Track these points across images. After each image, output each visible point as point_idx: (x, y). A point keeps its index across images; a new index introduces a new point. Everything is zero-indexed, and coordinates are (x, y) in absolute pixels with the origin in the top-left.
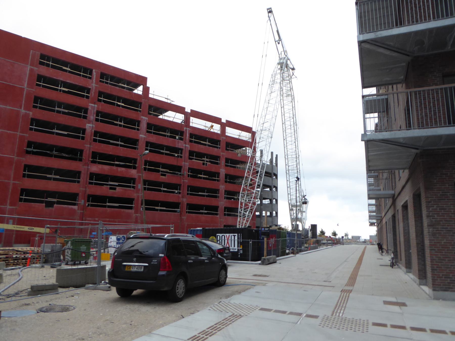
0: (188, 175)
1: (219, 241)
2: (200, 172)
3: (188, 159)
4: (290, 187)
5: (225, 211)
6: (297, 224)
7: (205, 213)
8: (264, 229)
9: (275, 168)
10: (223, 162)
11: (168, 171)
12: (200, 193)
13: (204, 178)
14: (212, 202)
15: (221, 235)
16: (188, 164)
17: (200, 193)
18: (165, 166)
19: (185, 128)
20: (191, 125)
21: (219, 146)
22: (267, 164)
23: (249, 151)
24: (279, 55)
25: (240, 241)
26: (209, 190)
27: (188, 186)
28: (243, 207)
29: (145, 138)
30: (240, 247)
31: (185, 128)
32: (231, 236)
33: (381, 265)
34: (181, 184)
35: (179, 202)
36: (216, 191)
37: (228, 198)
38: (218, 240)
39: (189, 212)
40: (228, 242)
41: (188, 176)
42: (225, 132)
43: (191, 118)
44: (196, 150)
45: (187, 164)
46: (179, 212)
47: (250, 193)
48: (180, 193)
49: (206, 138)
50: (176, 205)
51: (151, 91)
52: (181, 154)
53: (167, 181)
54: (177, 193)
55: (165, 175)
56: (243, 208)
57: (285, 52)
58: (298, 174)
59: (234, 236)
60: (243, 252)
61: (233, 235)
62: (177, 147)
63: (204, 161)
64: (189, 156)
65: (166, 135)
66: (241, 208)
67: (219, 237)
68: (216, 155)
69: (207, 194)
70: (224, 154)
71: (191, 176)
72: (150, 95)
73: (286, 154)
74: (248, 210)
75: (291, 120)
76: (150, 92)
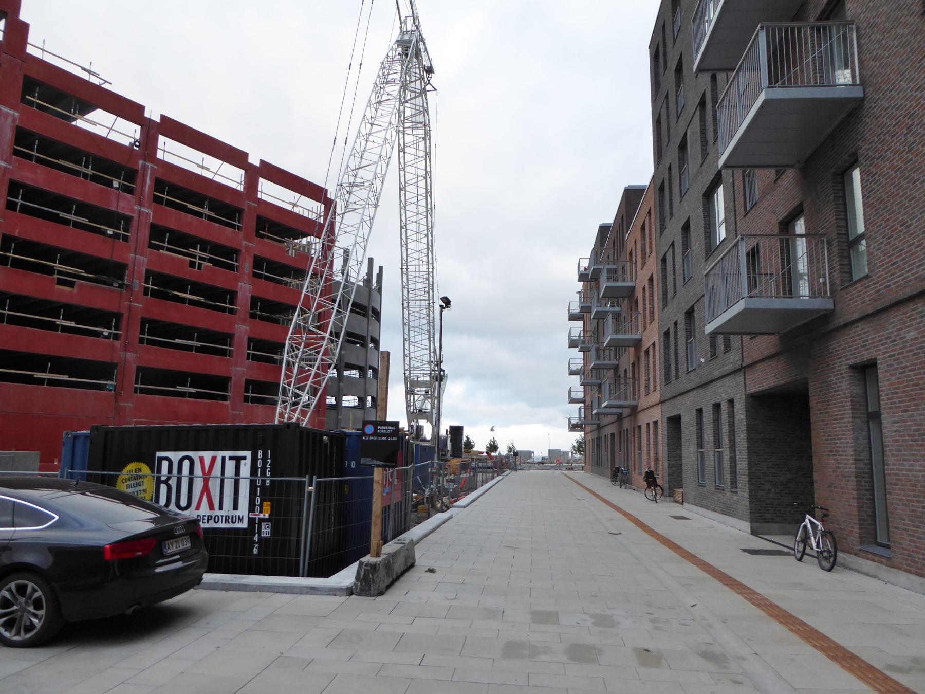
0: (146, 289)
1: (166, 482)
2: (181, 285)
3: (146, 246)
4: (409, 339)
5: (247, 391)
6: (420, 424)
7: (190, 393)
8: (376, 429)
9: (375, 294)
10: (247, 266)
11: (82, 272)
12: (177, 341)
13: (192, 302)
14: (214, 366)
15: (175, 456)
16: (146, 259)
17: (177, 341)
18: (70, 258)
19: (141, 162)
20: (160, 155)
21: (237, 223)
22: (358, 285)
23: (314, 244)
24: (401, 23)
25: (263, 482)
26: (205, 335)
27: (144, 322)
28: (295, 375)
29: (5, 168)
30: (261, 512)
31: (141, 162)
32: (224, 458)
33: (745, 551)
34: (122, 314)
35: (115, 362)
36: (226, 338)
37: (255, 358)
38: (163, 478)
39: (143, 391)
40: (206, 489)
41: (146, 293)
42: (257, 191)
43: (162, 139)
44: (173, 226)
45: (144, 259)
46: (111, 390)
47: (315, 339)
48: (116, 337)
49: (204, 198)
50: (104, 370)
51: (33, 37)
52: (126, 230)
53: (75, 301)
54: (106, 337)
55: (71, 284)
56: (294, 378)
57: (415, 17)
58: (429, 310)
59: (238, 460)
60: (275, 531)
61: (231, 458)
62: (113, 208)
63: (194, 257)
64: (151, 238)
65: (80, 172)
66: (288, 377)
67: (165, 464)
68: (228, 244)
69: (199, 344)
70: (250, 244)
71: (155, 294)
72: (29, 47)
73: (404, 262)
74: (306, 385)
75: (419, 184)
76: (30, 39)
